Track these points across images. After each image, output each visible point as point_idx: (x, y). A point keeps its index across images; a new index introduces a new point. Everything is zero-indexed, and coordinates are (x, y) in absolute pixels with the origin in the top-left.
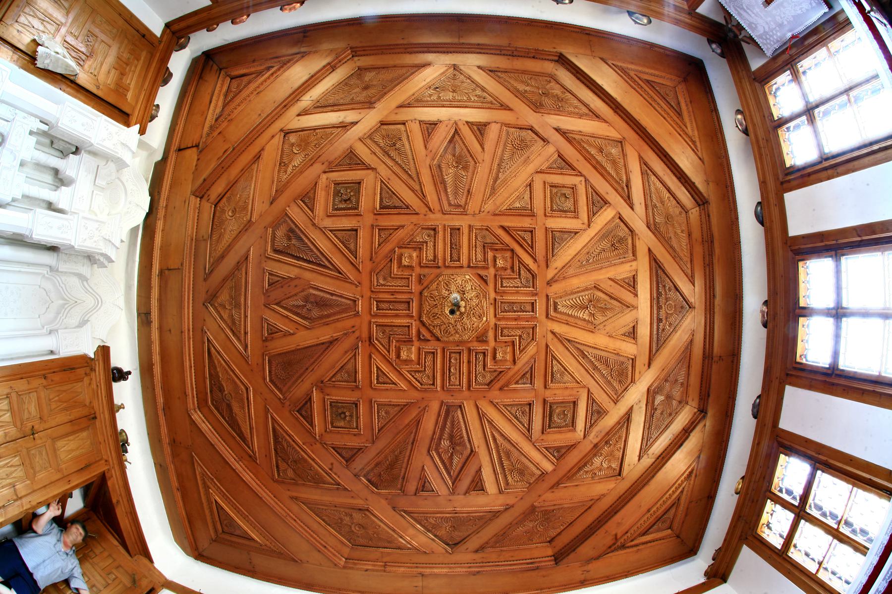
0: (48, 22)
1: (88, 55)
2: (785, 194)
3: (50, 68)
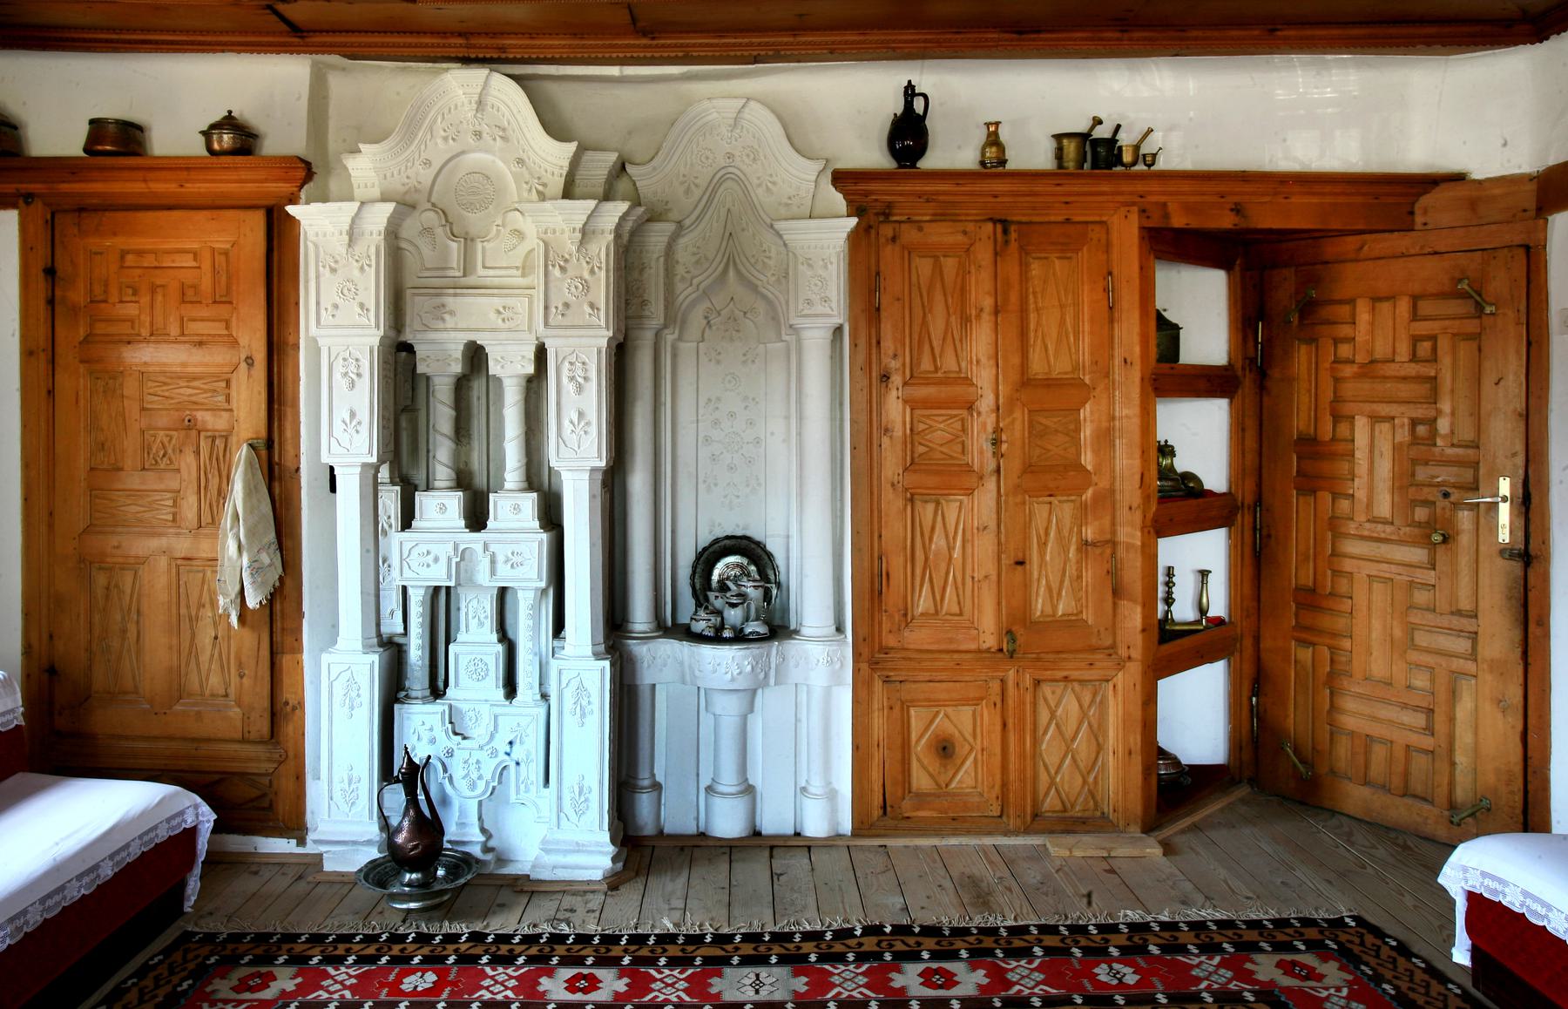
0: (188, 607)
1: (194, 433)
2: (1441, 880)
3: (272, 535)
